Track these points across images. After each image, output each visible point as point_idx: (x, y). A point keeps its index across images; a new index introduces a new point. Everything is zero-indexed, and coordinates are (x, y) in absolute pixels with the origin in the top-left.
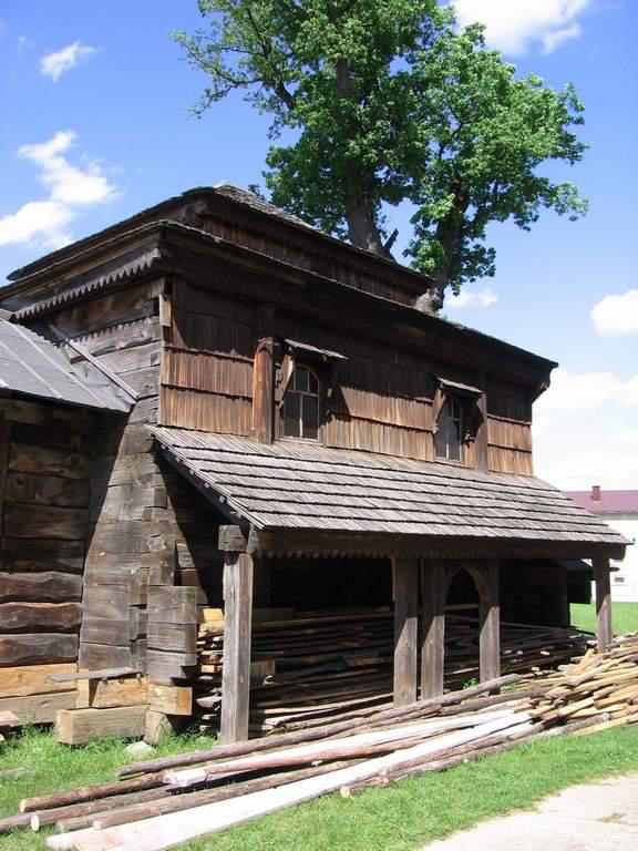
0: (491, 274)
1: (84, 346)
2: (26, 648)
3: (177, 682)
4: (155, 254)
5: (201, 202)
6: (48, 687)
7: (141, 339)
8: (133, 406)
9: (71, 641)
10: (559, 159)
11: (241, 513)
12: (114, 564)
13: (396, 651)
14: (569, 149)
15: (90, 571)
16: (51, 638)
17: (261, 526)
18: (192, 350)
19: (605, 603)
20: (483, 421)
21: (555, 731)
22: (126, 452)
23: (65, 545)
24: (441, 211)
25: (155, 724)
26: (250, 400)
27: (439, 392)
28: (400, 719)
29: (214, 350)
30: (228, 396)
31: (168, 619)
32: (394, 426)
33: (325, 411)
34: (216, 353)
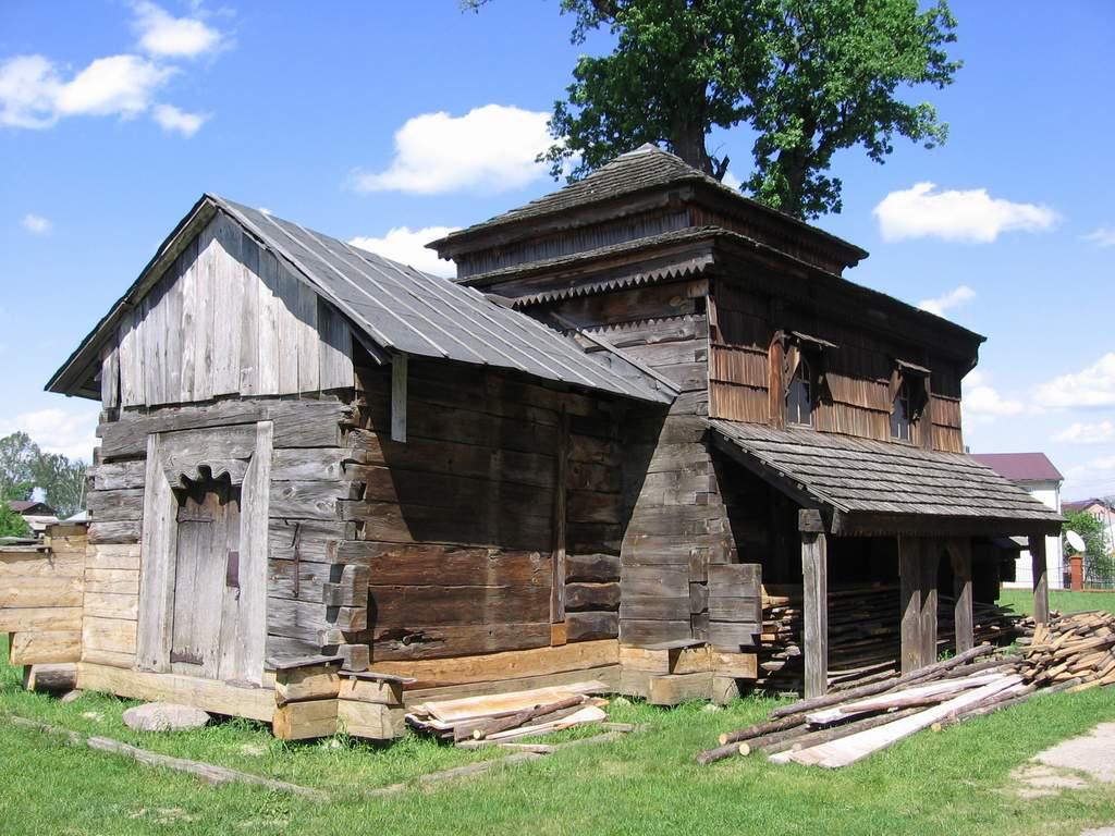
0: (837, 209)
1: (603, 337)
2: (585, 625)
3: (745, 649)
4: (709, 259)
5: (688, 189)
6: (600, 662)
7: (681, 336)
8: (675, 398)
9: (613, 616)
10: (928, 83)
11: (823, 498)
12: (660, 545)
13: (903, 622)
14: (940, 72)
15: (629, 553)
16: (601, 615)
17: (847, 511)
18: (729, 346)
19: (1042, 580)
20: (927, 400)
21: (1047, 690)
22: (670, 441)
23: (608, 529)
24: (789, 143)
25: (725, 688)
26: (766, 390)
27: (896, 373)
28: (923, 679)
29: (742, 345)
30: (752, 388)
31: (735, 593)
32: (863, 408)
33: (816, 397)
34: (744, 347)
